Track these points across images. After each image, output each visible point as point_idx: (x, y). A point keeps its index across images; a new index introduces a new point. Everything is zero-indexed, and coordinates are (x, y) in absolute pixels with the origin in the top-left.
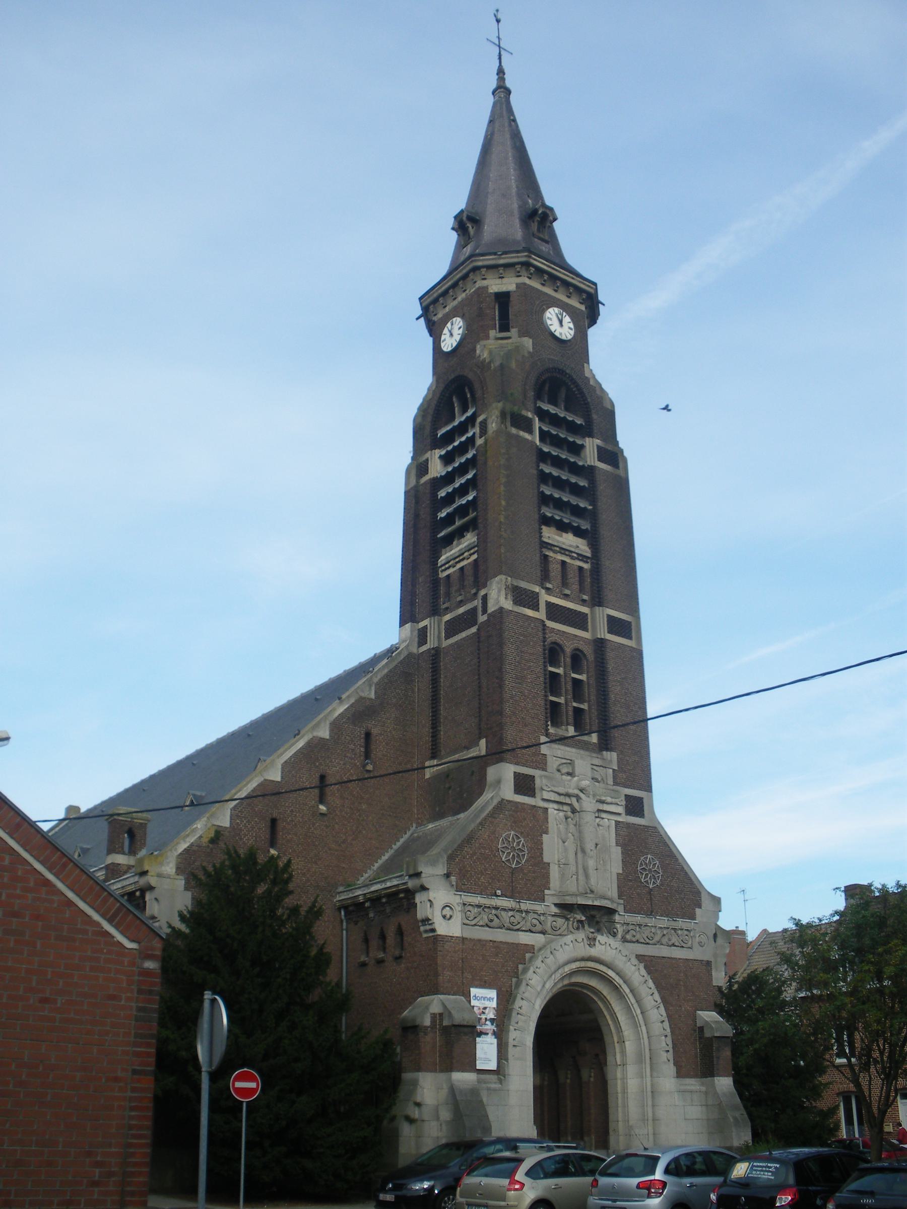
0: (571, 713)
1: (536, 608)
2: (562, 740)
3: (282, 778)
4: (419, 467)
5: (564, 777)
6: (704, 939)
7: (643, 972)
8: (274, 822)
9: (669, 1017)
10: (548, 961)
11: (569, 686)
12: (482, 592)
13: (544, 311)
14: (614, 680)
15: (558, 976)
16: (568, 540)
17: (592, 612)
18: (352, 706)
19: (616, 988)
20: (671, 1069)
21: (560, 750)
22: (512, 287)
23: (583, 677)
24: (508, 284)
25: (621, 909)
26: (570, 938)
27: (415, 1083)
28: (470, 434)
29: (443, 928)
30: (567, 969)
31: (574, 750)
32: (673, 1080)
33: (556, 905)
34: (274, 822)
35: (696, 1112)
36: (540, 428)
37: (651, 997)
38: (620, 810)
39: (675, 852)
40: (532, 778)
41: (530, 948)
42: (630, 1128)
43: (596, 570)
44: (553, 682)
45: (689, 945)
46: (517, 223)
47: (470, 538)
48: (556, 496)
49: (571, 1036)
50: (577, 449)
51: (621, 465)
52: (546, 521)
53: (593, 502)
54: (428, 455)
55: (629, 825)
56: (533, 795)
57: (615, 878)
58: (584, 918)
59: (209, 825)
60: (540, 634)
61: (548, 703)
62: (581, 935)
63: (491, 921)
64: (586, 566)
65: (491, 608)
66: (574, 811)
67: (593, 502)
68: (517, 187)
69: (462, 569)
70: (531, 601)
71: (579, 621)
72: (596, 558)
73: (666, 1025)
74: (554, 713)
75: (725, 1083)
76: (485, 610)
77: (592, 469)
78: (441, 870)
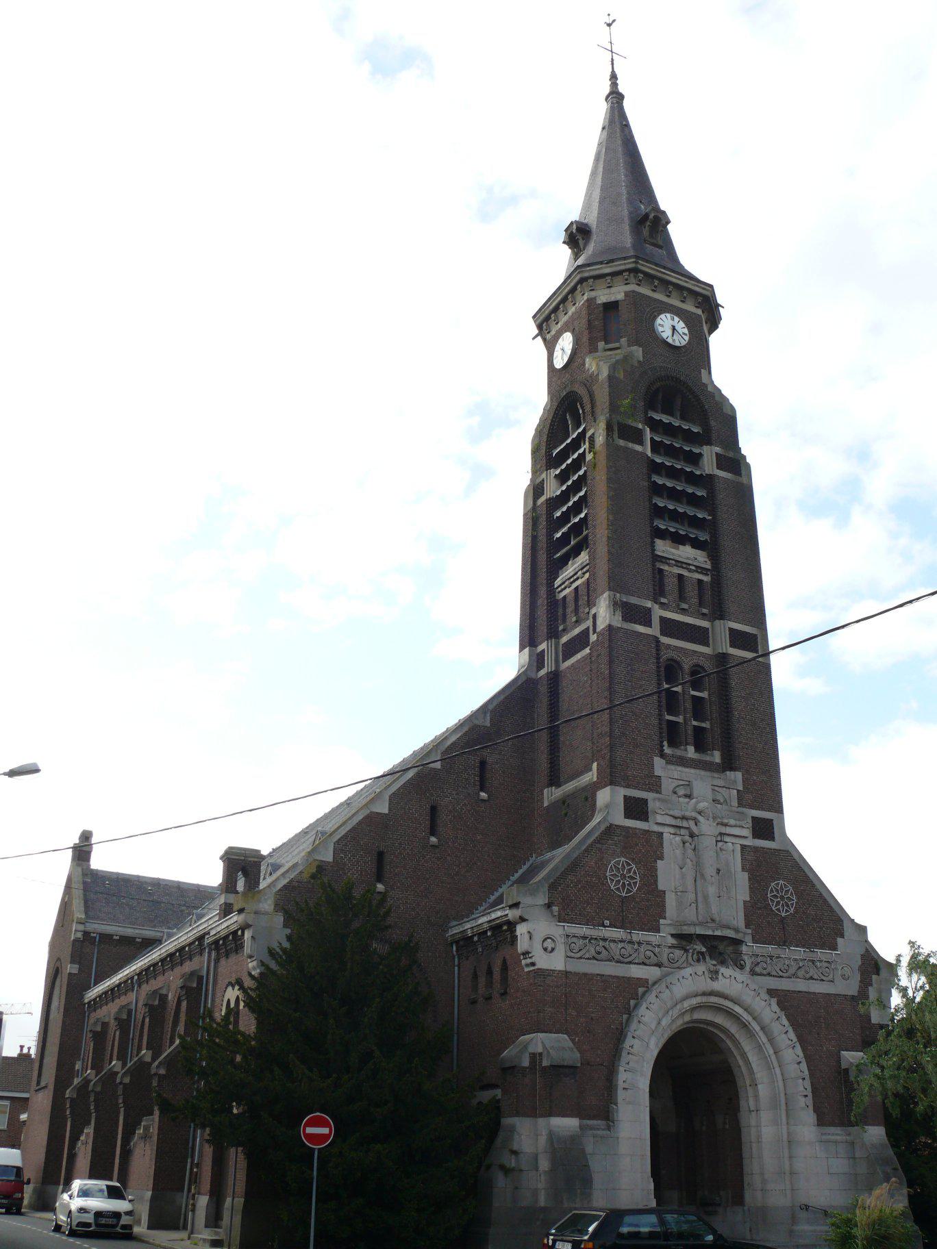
0: (690, 732)
1: (648, 623)
2: (683, 762)
3: (390, 809)
4: (536, 489)
5: (681, 799)
6: (847, 971)
7: (775, 1007)
8: (381, 855)
9: (808, 1057)
10: (663, 996)
11: (689, 705)
12: (593, 611)
13: (655, 318)
14: (737, 695)
15: (676, 1012)
16: (686, 552)
17: (712, 626)
18: (465, 734)
19: (744, 1026)
20: (810, 1117)
21: (678, 772)
22: (620, 297)
23: (705, 695)
24: (617, 293)
25: (748, 939)
26: (689, 970)
27: (512, 1129)
28: (581, 451)
29: (543, 961)
30: (687, 1004)
31: (693, 771)
32: (814, 1129)
33: (672, 935)
34: (381, 855)
35: (840, 1164)
36: (652, 439)
37: (785, 1035)
38: (746, 832)
39: (811, 876)
40: (645, 801)
41: (643, 982)
42: (764, 1182)
43: (717, 582)
44: (671, 702)
45: (830, 977)
46: (626, 228)
47: (584, 557)
48: (671, 507)
49: (698, 1079)
50: (695, 459)
51: (743, 472)
52: (662, 534)
53: (713, 512)
54: (544, 475)
55: (756, 849)
56: (646, 820)
57: (741, 905)
58: (704, 950)
59: (311, 860)
60: (654, 651)
61: (664, 726)
62: (701, 968)
63: (599, 953)
64: (706, 579)
65: (601, 626)
66: (692, 835)
67: (713, 512)
68: (628, 193)
69: (577, 589)
70: (644, 617)
71: (700, 636)
72: (716, 570)
73: (804, 1066)
74: (673, 734)
75: (876, 1133)
76: (594, 631)
77: (711, 477)
78: (542, 899)
